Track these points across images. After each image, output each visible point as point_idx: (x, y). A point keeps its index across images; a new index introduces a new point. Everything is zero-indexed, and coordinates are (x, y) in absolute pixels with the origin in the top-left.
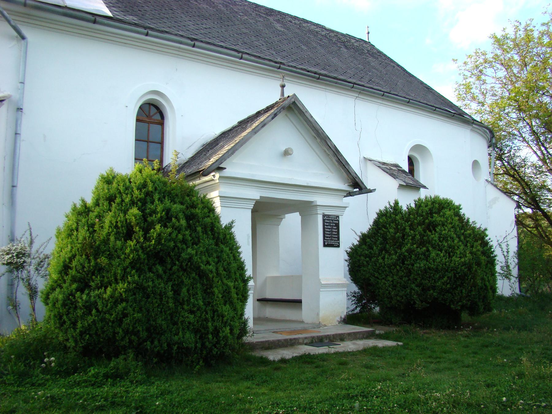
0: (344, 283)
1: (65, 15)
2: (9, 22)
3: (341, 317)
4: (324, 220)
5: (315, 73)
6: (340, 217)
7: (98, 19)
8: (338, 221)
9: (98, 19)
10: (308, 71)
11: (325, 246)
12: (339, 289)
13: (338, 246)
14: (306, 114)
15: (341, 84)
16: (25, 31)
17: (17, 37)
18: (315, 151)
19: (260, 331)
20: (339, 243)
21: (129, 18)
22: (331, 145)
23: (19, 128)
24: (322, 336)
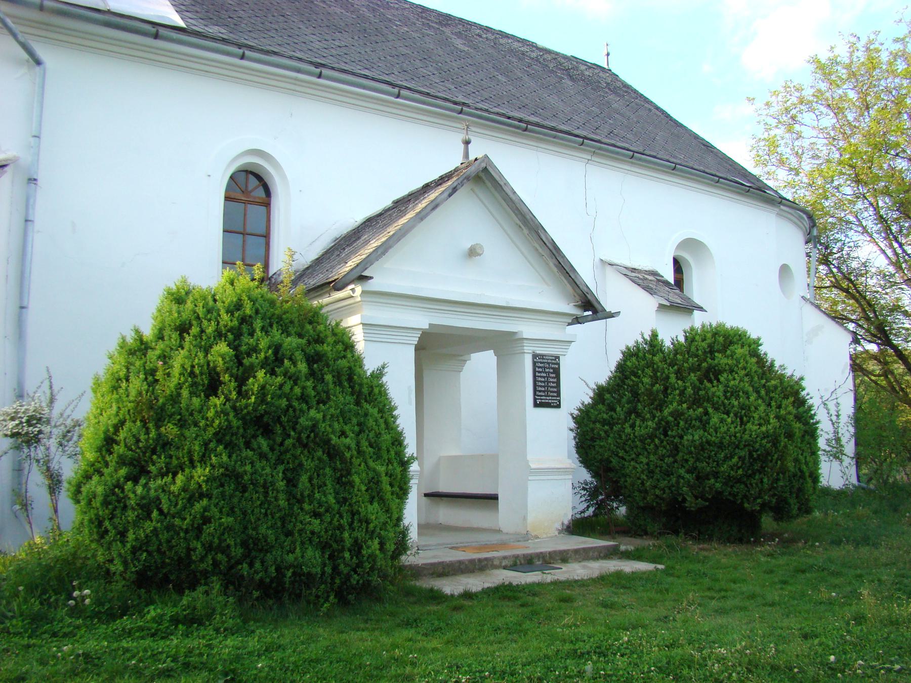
0: (568, 466)
1: (108, 25)
2: (15, 36)
3: (563, 524)
4: (534, 363)
5: (520, 121)
6: (561, 358)
7: (162, 31)
8: (559, 364)
9: (162, 31)
10: (509, 118)
11: (536, 405)
12: (560, 477)
13: (558, 406)
14: (505, 188)
16: (41, 51)
17: (27, 61)
18: (520, 250)
19: (429, 545)
20: (559, 401)
21: (213, 30)
22: (547, 238)
23: (31, 211)
24: (531, 555)
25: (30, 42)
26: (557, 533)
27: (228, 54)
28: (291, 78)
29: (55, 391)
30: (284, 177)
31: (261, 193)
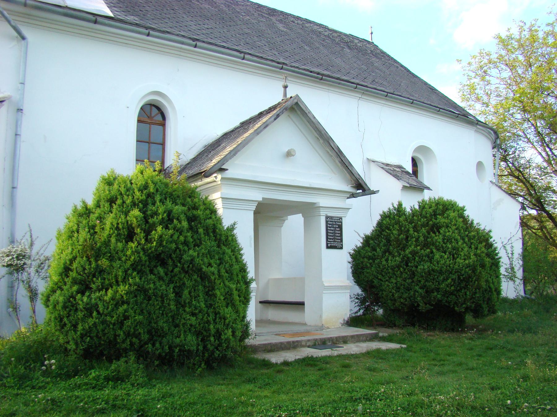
0: (347, 285)
1: (66, 15)
2: (9, 22)
3: (344, 320)
4: (327, 222)
5: (318, 74)
6: (343, 218)
7: (99, 19)
8: (341, 222)
9: (99, 19)
10: (311, 72)
11: (328, 247)
12: (342, 291)
13: (341, 248)
14: (309, 115)
15: (344, 85)
16: (25, 31)
17: (17, 37)
18: (318, 153)
19: (262, 333)
20: (342, 245)
21: (130, 18)
22: (334, 145)
23: (19, 129)
24: (325, 339)
25: (18, 26)
26: (340, 325)
27: (139, 33)
28: (178, 48)
29: (34, 239)
30: (173, 108)
31: (159, 118)
